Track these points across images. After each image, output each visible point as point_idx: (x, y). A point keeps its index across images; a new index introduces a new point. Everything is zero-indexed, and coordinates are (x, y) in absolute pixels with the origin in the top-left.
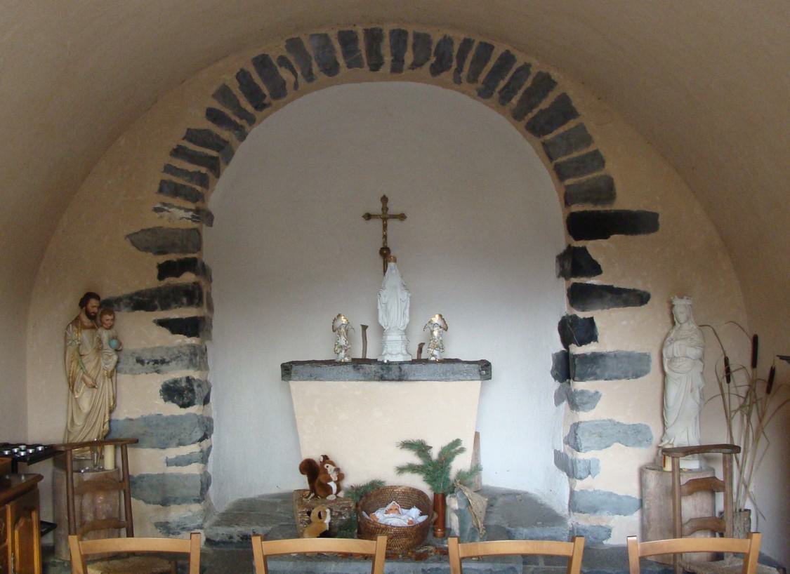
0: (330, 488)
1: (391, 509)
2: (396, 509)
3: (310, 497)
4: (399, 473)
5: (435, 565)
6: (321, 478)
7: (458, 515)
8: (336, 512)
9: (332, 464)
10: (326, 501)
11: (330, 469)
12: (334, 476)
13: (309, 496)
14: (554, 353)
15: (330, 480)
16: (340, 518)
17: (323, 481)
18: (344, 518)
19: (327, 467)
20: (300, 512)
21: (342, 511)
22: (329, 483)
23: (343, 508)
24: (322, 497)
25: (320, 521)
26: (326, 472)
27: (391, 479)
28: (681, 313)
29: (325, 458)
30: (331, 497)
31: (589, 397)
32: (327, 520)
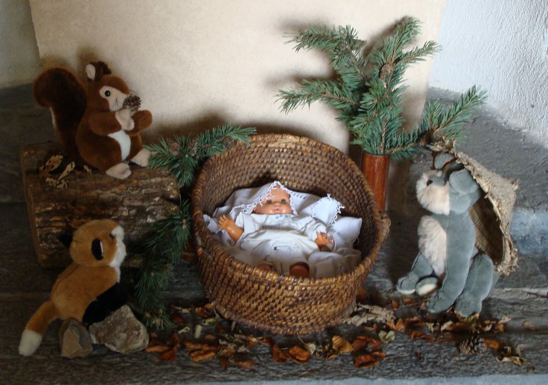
0: (116, 147)
1: (269, 202)
2: (283, 202)
3: (65, 173)
4: (306, 256)
5: (492, 273)
6: (92, 121)
7: (448, 229)
8: (131, 207)
9: (121, 85)
10: (104, 181)
11: (115, 99)
12: (125, 119)
13: (61, 169)
14: (431, 85)
15: (116, 127)
16: (142, 221)
17: (99, 131)
18: (150, 220)
19: (108, 93)
20: (39, 215)
21: (146, 204)
22: (112, 135)
23: (149, 197)
24: (94, 170)
25: (96, 263)
26: (103, 107)
27: (252, 103)
28: (476, 382)
29: (103, 68)
30: (119, 171)
31: (501, 158)
32: (118, 258)
